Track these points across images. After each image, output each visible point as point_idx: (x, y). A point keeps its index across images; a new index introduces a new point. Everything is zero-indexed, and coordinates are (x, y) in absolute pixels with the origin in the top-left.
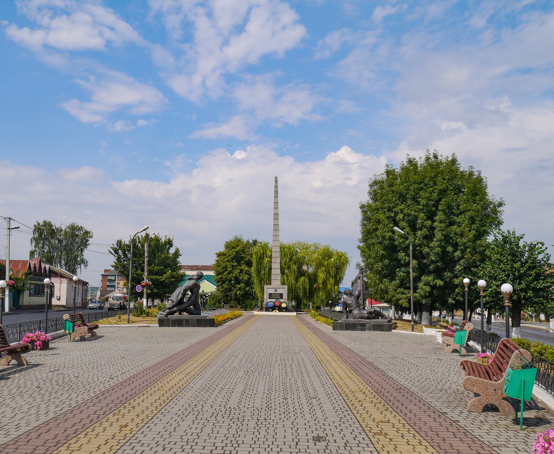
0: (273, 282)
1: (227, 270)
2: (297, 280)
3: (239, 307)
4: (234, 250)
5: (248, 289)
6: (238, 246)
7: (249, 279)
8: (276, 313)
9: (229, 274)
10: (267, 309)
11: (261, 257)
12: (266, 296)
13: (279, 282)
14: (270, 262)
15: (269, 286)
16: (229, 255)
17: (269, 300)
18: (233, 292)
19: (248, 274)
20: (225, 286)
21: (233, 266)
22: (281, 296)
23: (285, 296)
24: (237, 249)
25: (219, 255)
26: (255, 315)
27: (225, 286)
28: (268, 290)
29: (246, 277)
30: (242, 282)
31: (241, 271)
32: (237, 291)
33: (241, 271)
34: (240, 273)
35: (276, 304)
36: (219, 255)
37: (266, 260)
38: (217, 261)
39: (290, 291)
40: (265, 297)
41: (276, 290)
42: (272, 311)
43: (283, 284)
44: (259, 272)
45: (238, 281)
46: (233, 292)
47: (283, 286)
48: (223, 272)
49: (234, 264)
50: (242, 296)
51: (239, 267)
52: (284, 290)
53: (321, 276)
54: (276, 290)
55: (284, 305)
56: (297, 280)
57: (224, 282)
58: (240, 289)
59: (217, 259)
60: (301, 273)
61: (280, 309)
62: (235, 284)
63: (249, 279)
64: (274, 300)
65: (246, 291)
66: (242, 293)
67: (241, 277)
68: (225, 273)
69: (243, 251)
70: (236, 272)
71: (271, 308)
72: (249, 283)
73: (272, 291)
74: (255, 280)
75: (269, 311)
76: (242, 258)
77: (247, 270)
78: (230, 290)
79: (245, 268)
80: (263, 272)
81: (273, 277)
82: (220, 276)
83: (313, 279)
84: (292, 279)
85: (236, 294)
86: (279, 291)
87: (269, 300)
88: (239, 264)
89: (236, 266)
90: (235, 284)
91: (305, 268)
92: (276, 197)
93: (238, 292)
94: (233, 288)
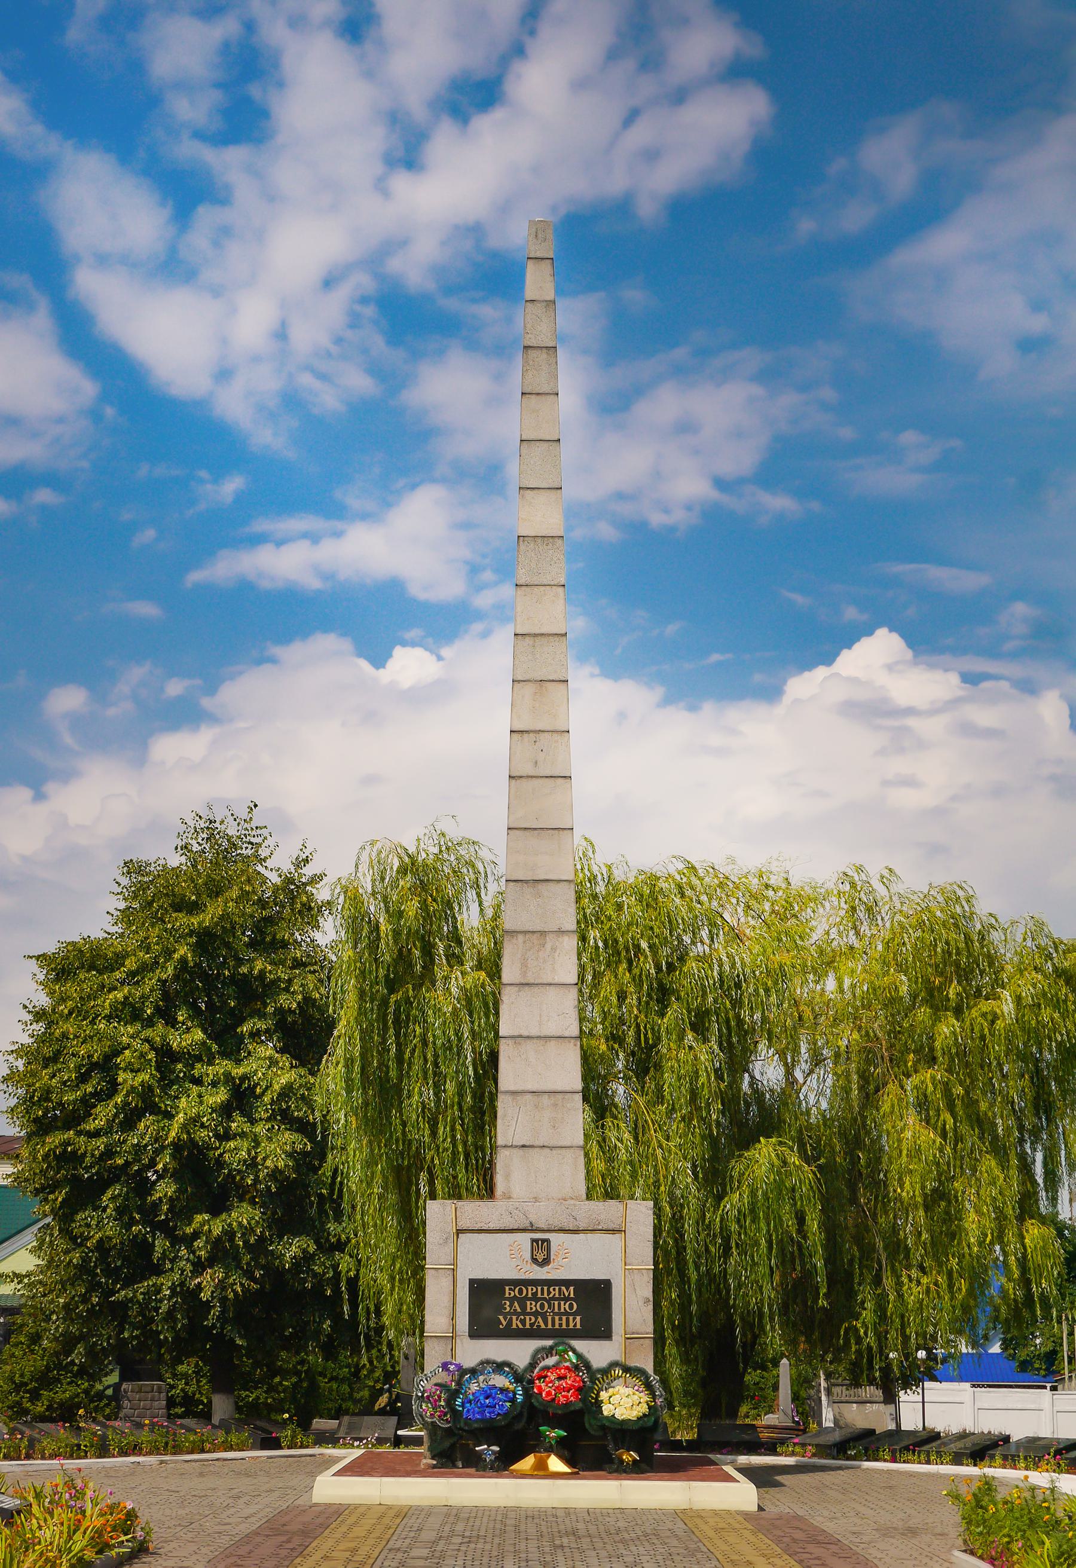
0: (512, 1172)
1: (113, 1087)
2: (715, 1177)
3: (221, 1406)
4: (183, 920)
5: (292, 1249)
6: (215, 890)
7: (308, 1162)
8: (546, 1488)
9: (129, 1119)
10: (454, 1451)
11: (402, 958)
12: (444, 1307)
13: (568, 1174)
14: (485, 1005)
15: (473, 1211)
16: (144, 969)
17: (472, 1352)
18: (166, 1283)
19: (304, 1127)
20: (102, 1223)
21: (166, 1055)
22: (593, 1300)
23: (633, 1307)
24: (206, 918)
25: (65, 967)
26: (336, 1512)
27: (102, 1223)
28: (466, 1246)
29: (277, 1149)
30: (243, 1194)
31: (242, 1097)
32: (199, 1267)
33: (242, 1097)
34: (226, 1111)
35: (545, 1389)
36: (65, 967)
37: (456, 983)
38: (39, 1015)
39: (669, 1261)
40: (436, 1320)
41: (541, 1252)
42: (503, 1464)
43: (605, 1188)
44: (382, 1092)
45: (204, 1179)
46: (166, 1283)
47: (607, 1211)
48: (87, 1106)
49: (177, 1041)
50: (241, 1310)
51: (222, 1066)
52: (618, 1252)
53: (909, 1138)
54: (541, 1252)
55: (623, 1402)
56: (715, 1177)
57: (86, 1193)
58: (222, 1252)
59: (43, 1000)
60: (750, 1120)
61: (594, 1446)
62: (182, 1210)
63: (308, 1162)
64: (519, 1352)
65: (276, 1275)
66: (238, 1283)
67: (235, 1152)
68: (102, 1115)
69: (264, 938)
70: (195, 1105)
71: (489, 1431)
72: (303, 1198)
73: (503, 1260)
74: (354, 1161)
75: (474, 1464)
76: (253, 993)
77: (287, 1092)
78: (140, 1262)
79: (266, 1065)
80: (419, 1094)
81: (512, 1124)
82: (54, 1140)
83: (848, 1162)
84: (677, 1156)
85: (189, 1296)
86: (577, 1260)
87: (472, 1352)
88: (227, 1041)
89: (192, 1058)
90: (182, 1210)
91: (767, 1070)
92: (528, 777)
93: (208, 1282)
94: (161, 1244)
